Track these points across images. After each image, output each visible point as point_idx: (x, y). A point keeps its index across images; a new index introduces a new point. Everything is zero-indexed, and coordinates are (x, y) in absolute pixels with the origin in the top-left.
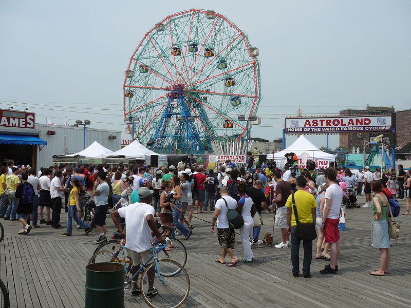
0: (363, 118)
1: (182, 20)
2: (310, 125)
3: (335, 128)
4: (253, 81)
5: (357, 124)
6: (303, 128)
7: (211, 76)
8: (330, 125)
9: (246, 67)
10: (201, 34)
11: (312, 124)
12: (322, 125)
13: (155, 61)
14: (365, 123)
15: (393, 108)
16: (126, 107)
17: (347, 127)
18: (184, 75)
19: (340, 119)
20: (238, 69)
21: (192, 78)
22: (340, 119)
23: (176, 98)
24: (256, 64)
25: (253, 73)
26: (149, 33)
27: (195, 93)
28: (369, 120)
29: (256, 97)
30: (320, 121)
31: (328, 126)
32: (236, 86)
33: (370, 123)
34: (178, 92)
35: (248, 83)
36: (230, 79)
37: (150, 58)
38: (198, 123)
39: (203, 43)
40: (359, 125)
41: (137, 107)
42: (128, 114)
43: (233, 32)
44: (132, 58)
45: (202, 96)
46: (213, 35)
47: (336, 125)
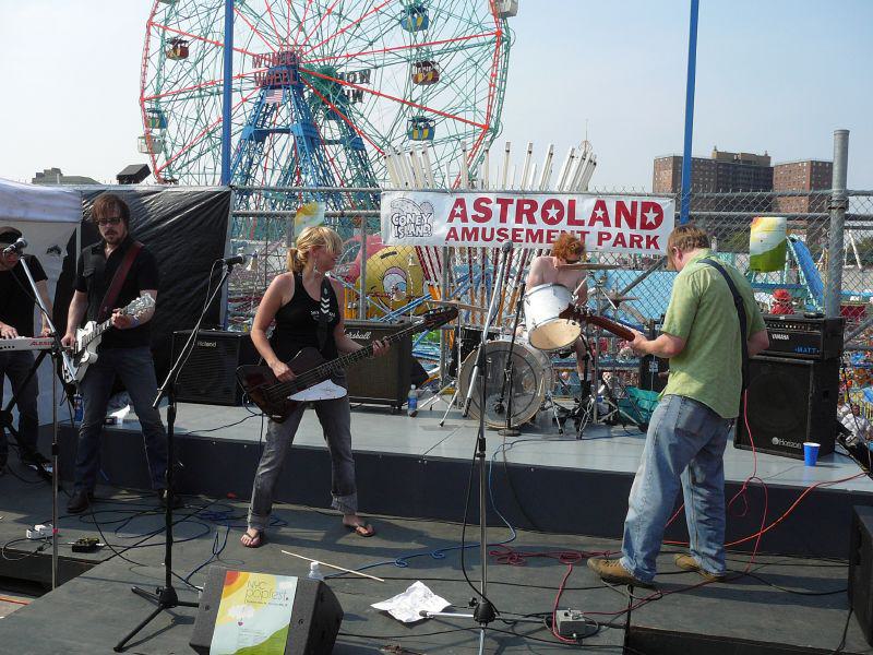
4: (485, 84)
7: (378, 46)
9: (473, 41)
11: (471, 211)
12: (503, 219)
14: (644, 218)
15: (767, 158)
16: (148, 82)
18: (309, 26)
19: (565, 200)
20: (453, 41)
21: (328, 40)
23: (279, 87)
24: (502, 40)
25: (490, 62)
29: (486, 128)
30: (499, 201)
32: (441, 85)
34: (286, 73)
35: (471, 86)
36: (426, 64)
38: (338, 156)
41: (176, 88)
42: (150, 99)
44: (150, 24)
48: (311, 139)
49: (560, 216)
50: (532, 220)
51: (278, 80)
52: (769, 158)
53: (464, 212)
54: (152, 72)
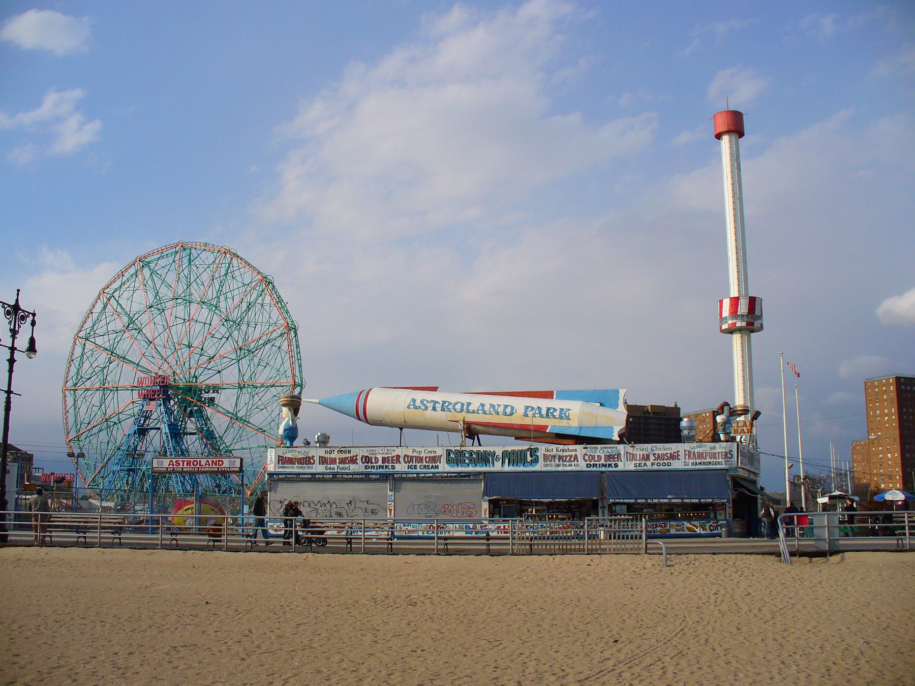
0: (218, 459)
1: (162, 262)
2: (173, 465)
3: (194, 468)
5: (212, 465)
6: (167, 468)
8: (190, 465)
10: (194, 284)
11: (175, 464)
12: (183, 465)
13: (119, 338)
14: (219, 464)
16: (70, 377)
17: (204, 468)
19: (198, 460)
22: (198, 460)
23: (154, 400)
26: (105, 289)
27: (192, 391)
28: (222, 461)
31: (189, 466)
33: (223, 464)
37: (108, 333)
39: (199, 300)
40: (214, 466)
43: (248, 276)
45: (206, 395)
46: (217, 283)
47: (195, 465)
48: (176, 433)
49: (197, 464)
50: (190, 465)
51: (154, 395)
52: (679, 408)
53: (173, 463)
54: (73, 370)
